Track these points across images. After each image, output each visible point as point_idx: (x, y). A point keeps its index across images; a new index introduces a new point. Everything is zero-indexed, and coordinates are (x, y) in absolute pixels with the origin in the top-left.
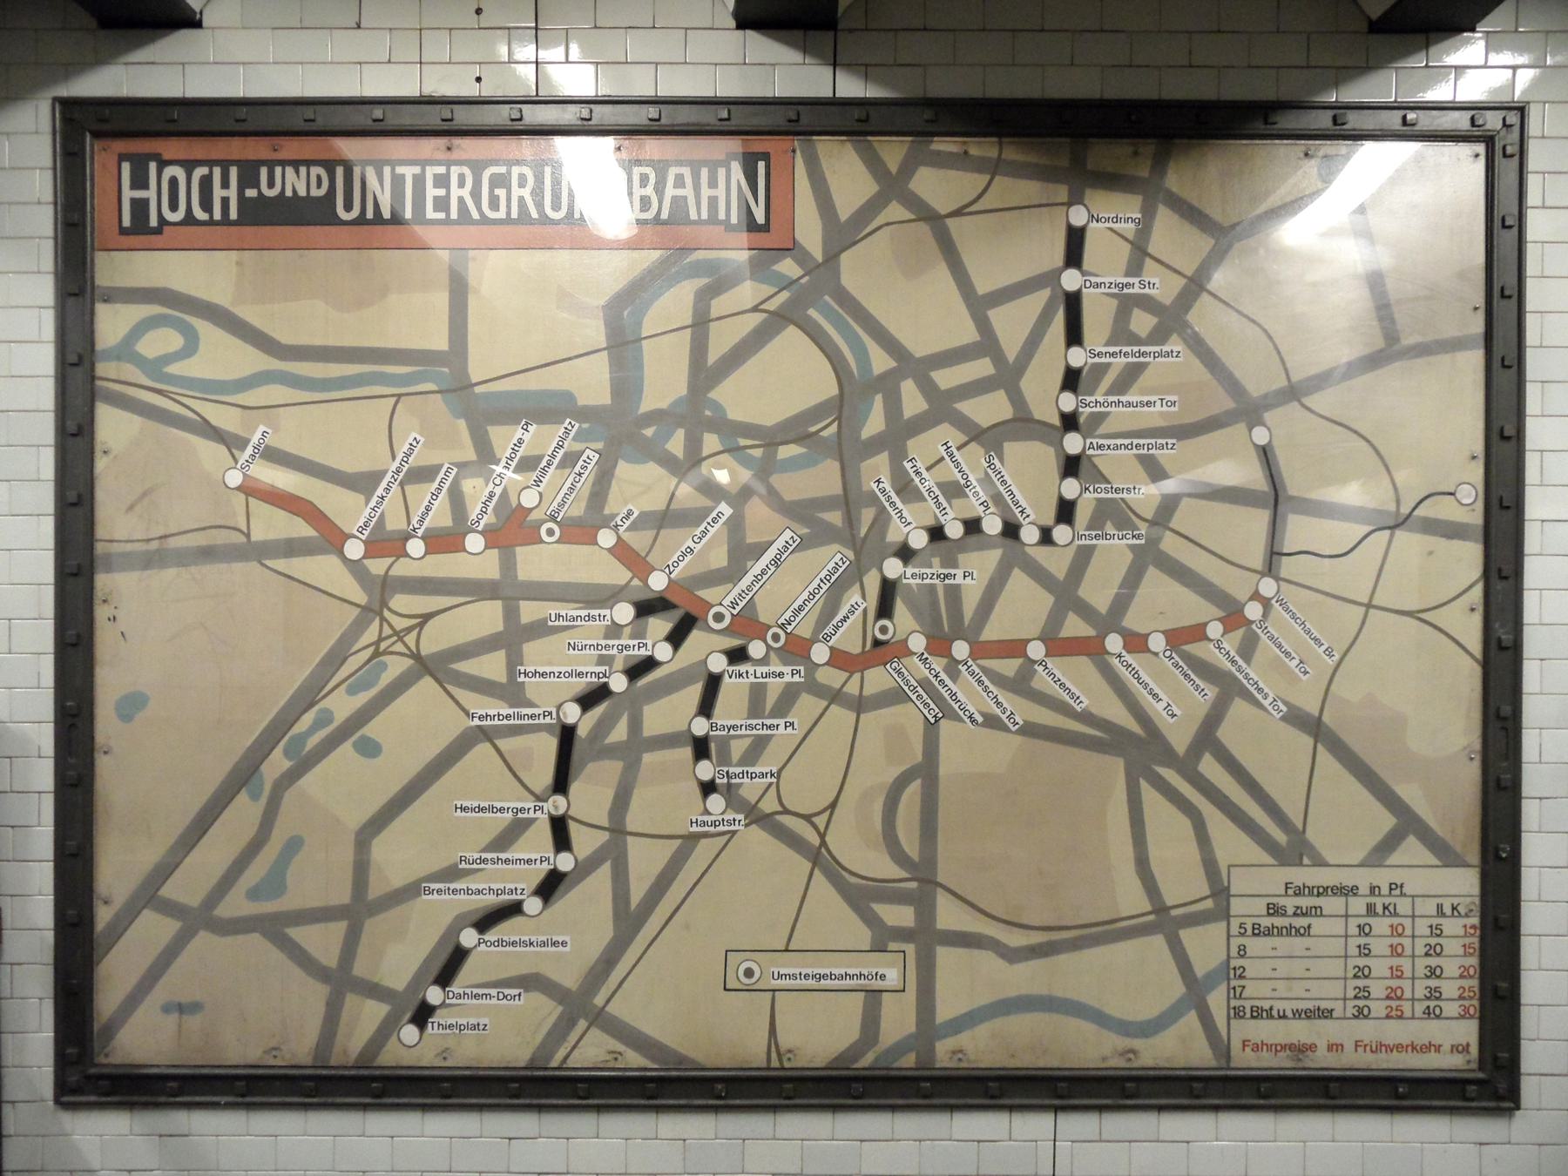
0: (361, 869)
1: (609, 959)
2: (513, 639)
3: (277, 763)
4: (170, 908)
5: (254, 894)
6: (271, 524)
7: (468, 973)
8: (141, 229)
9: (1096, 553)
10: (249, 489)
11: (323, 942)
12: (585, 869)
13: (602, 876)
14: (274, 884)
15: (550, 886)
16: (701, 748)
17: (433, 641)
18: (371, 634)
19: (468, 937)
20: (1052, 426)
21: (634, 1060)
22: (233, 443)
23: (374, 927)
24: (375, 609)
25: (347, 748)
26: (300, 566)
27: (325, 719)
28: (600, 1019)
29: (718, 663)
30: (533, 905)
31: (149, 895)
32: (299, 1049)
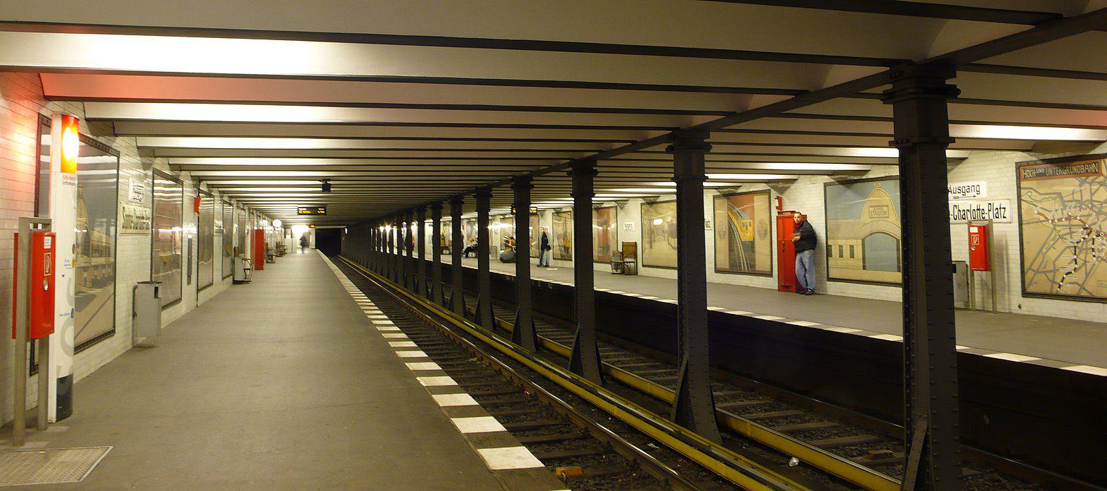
0: (1054, 265)
1: (1085, 281)
2: (1071, 233)
3: (1044, 250)
4: (1033, 271)
5: (1043, 268)
6: (1042, 218)
7: (1065, 281)
8: (1025, 179)
9: (96, 300)
10: (1039, 213)
11: (1050, 275)
12: (1080, 268)
13: (1084, 267)
14: (1045, 267)
15: (1075, 270)
16: (1093, 250)
17: (1061, 233)
18: (1054, 232)
19: (1065, 276)
20: (39, 377)
21: (1088, 295)
22: (1036, 206)
23: (1057, 272)
24: (1054, 229)
25: (1052, 249)
26: (1045, 223)
27: (613, 233)
28: (1084, 289)
29: (1095, 237)
30: (1073, 272)
31: (1030, 268)
32: (1048, 291)
